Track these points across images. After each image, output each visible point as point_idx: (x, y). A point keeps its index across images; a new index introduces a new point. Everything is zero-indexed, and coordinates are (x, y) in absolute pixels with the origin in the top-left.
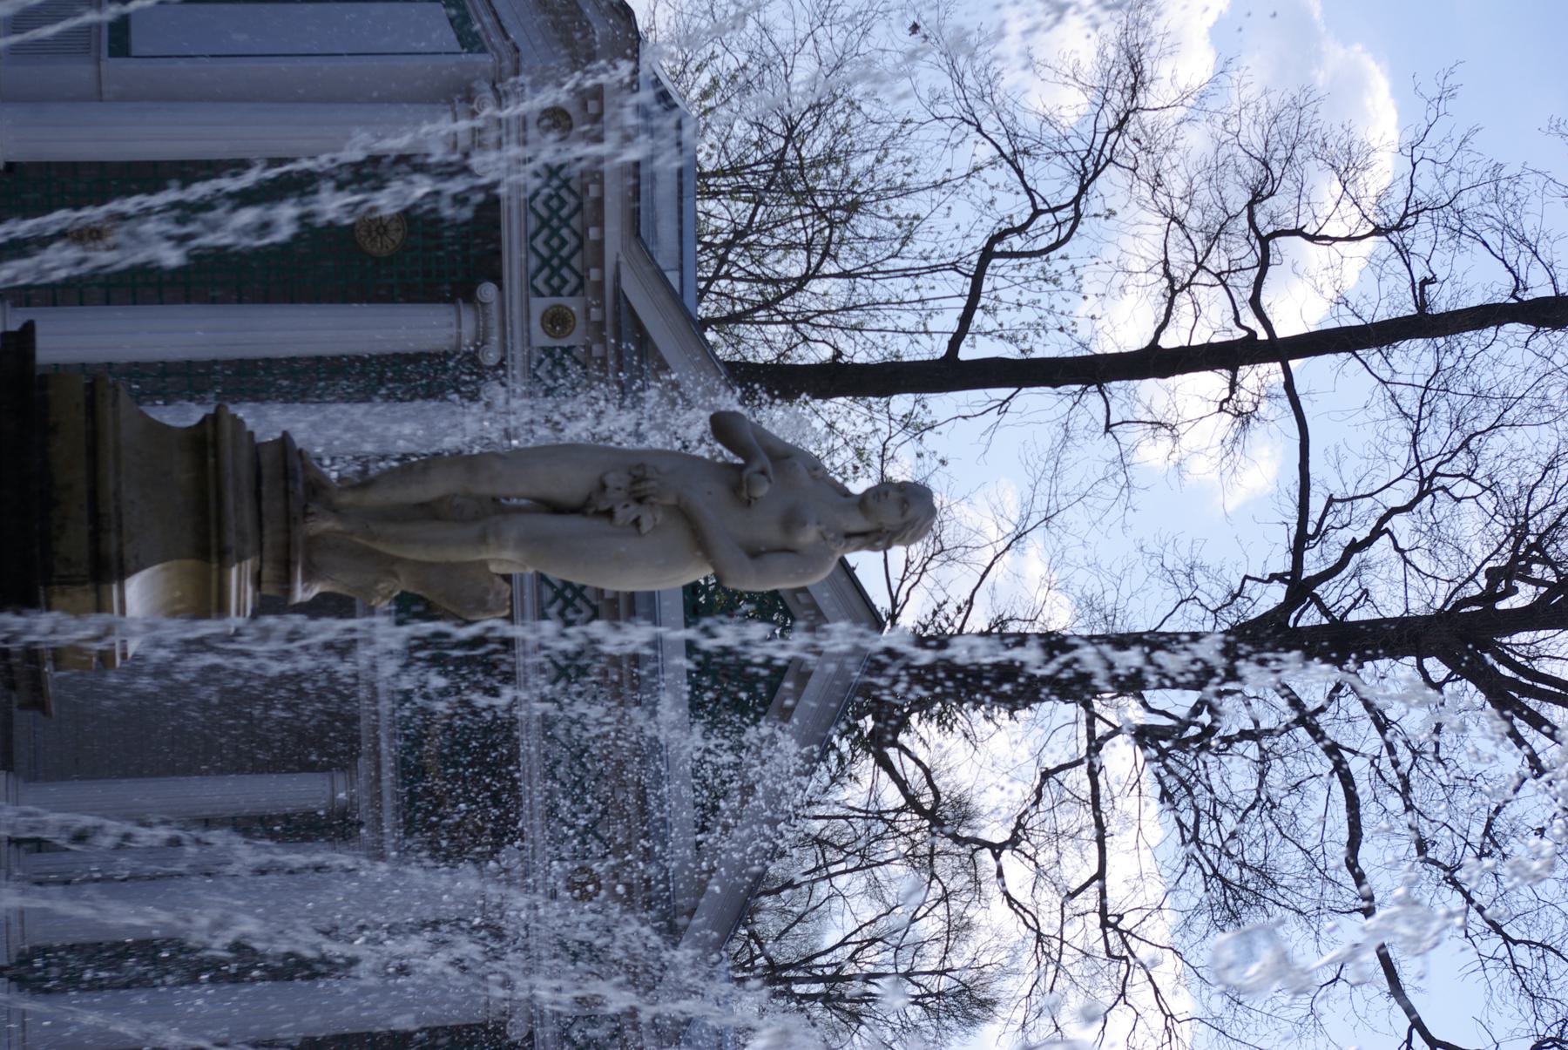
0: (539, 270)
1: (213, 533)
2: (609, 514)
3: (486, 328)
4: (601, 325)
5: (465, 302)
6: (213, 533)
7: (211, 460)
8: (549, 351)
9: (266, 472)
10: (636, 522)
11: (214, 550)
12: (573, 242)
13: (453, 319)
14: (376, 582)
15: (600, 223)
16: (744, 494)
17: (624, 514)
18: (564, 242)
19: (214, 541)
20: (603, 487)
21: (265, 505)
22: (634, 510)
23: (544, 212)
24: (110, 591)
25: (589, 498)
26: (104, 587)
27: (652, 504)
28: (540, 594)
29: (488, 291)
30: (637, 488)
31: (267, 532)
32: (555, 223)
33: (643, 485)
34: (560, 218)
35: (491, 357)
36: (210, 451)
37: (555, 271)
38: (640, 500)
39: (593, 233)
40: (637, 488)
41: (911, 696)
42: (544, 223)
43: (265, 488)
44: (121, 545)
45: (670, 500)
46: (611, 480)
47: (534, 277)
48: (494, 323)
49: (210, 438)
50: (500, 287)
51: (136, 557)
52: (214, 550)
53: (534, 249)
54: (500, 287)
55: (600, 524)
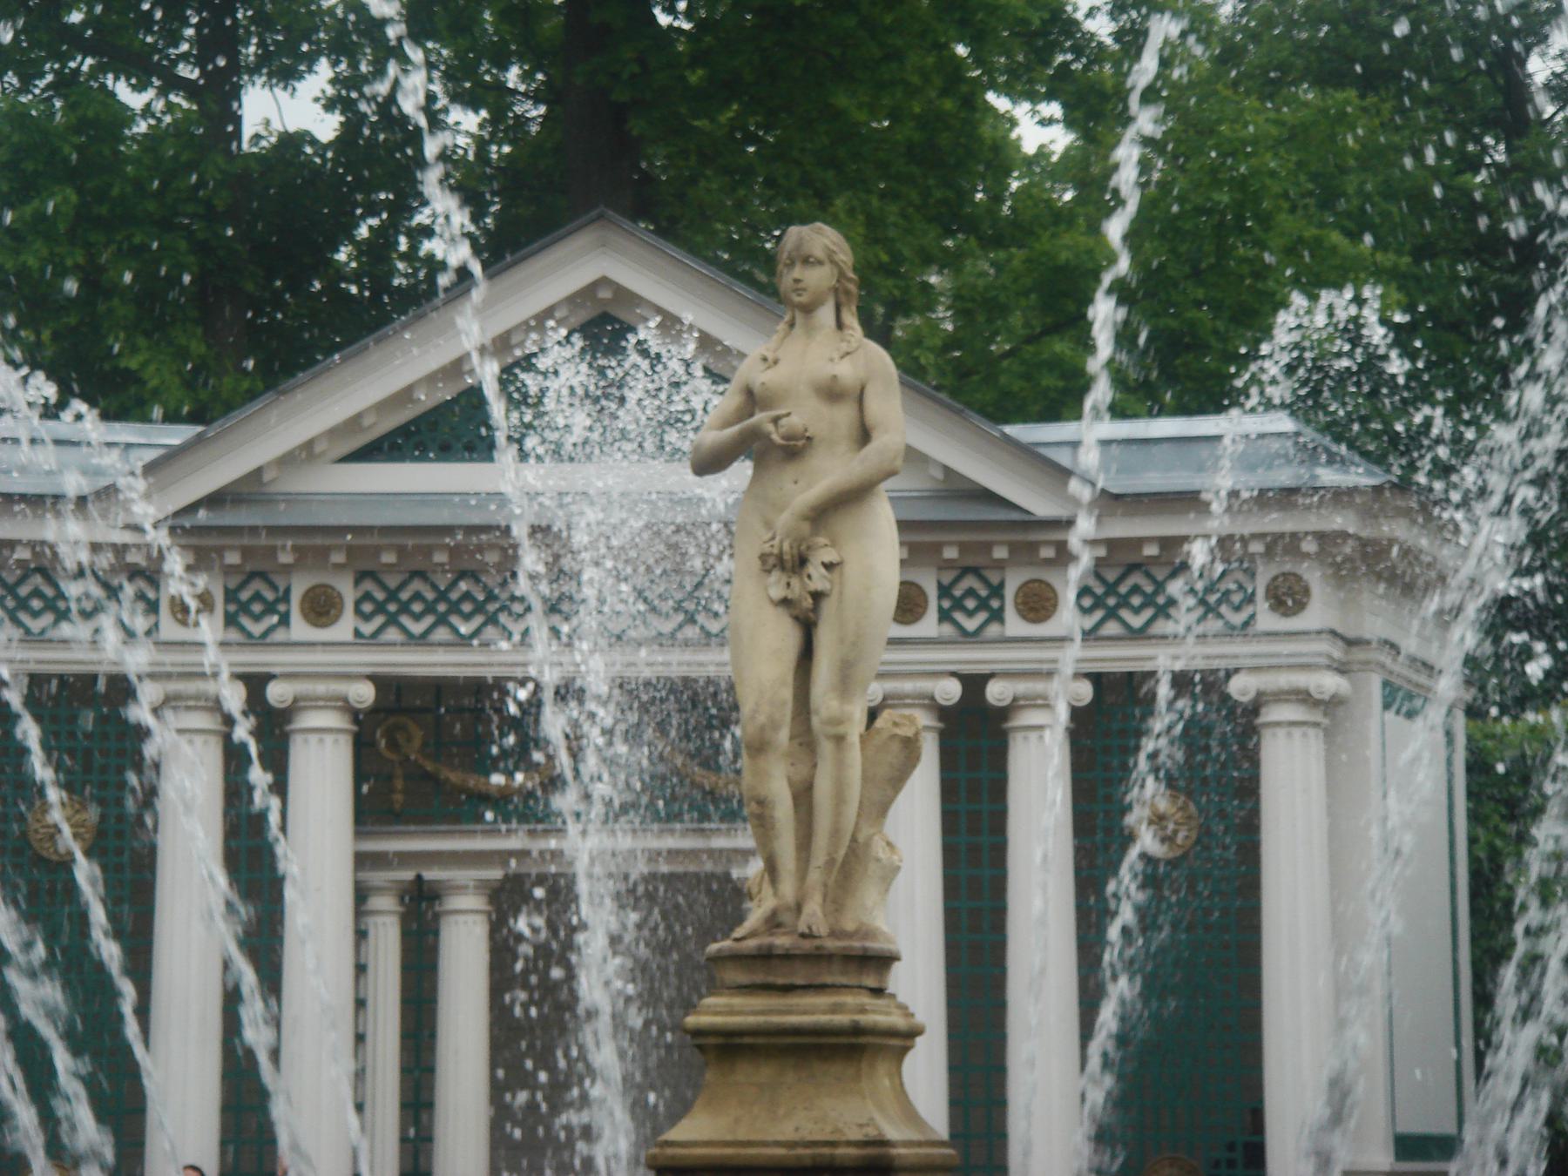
0: (242, 629)
1: (833, 1040)
2: (817, 596)
3: (197, 697)
4: (1014, 548)
5: (289, 721)
6: (833, 1040)
7: (747, 1040)
8: (944, 616)
9: (759, 978)
10: (829, 566)
11: (853, 1040)
12: (257, 585)
13: (1281, 732)
14: (878, 860)
15: (1139, 542)
16: (800, 443)
17: (818, 578)
18: (257, 597)
19: (843, 1040)
20: (785, 602)
21: (799, 981)
22: (815, 569)
23: (379, 620)
24: (899, 1155)
25: (796, 618)
26: (897, 1163)
27: (809, 548)
28: (687, 644)
29: (1241, 687)
30: (789, 565)
31: (829, 980)
32: (442, 608)
33: (787, 557)
34: (436, 601)
35: (950, 691)
36: (737, 1040)
37: (23, 604)
38: (802, 561)
39: (1151, 550)
40: (789, 565)
41: (1192, 314)
42: (392, 620)
43: (780, 981)
44: (849, 1143)
45: (806, 527)
46: (777, 592)
47: (249, 635)
48: (321, 688)
49: (720, 1040)
50: (992, 675)
51: (861, 1126)
52: (853, 1040)
53: (477, 633)
54: (992, 675)
55: (828, 607)
